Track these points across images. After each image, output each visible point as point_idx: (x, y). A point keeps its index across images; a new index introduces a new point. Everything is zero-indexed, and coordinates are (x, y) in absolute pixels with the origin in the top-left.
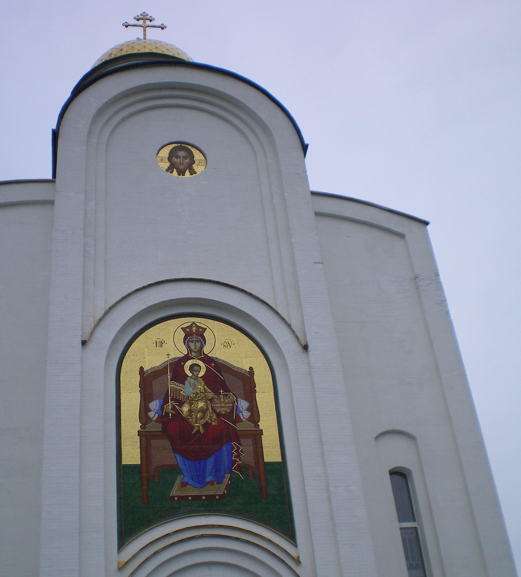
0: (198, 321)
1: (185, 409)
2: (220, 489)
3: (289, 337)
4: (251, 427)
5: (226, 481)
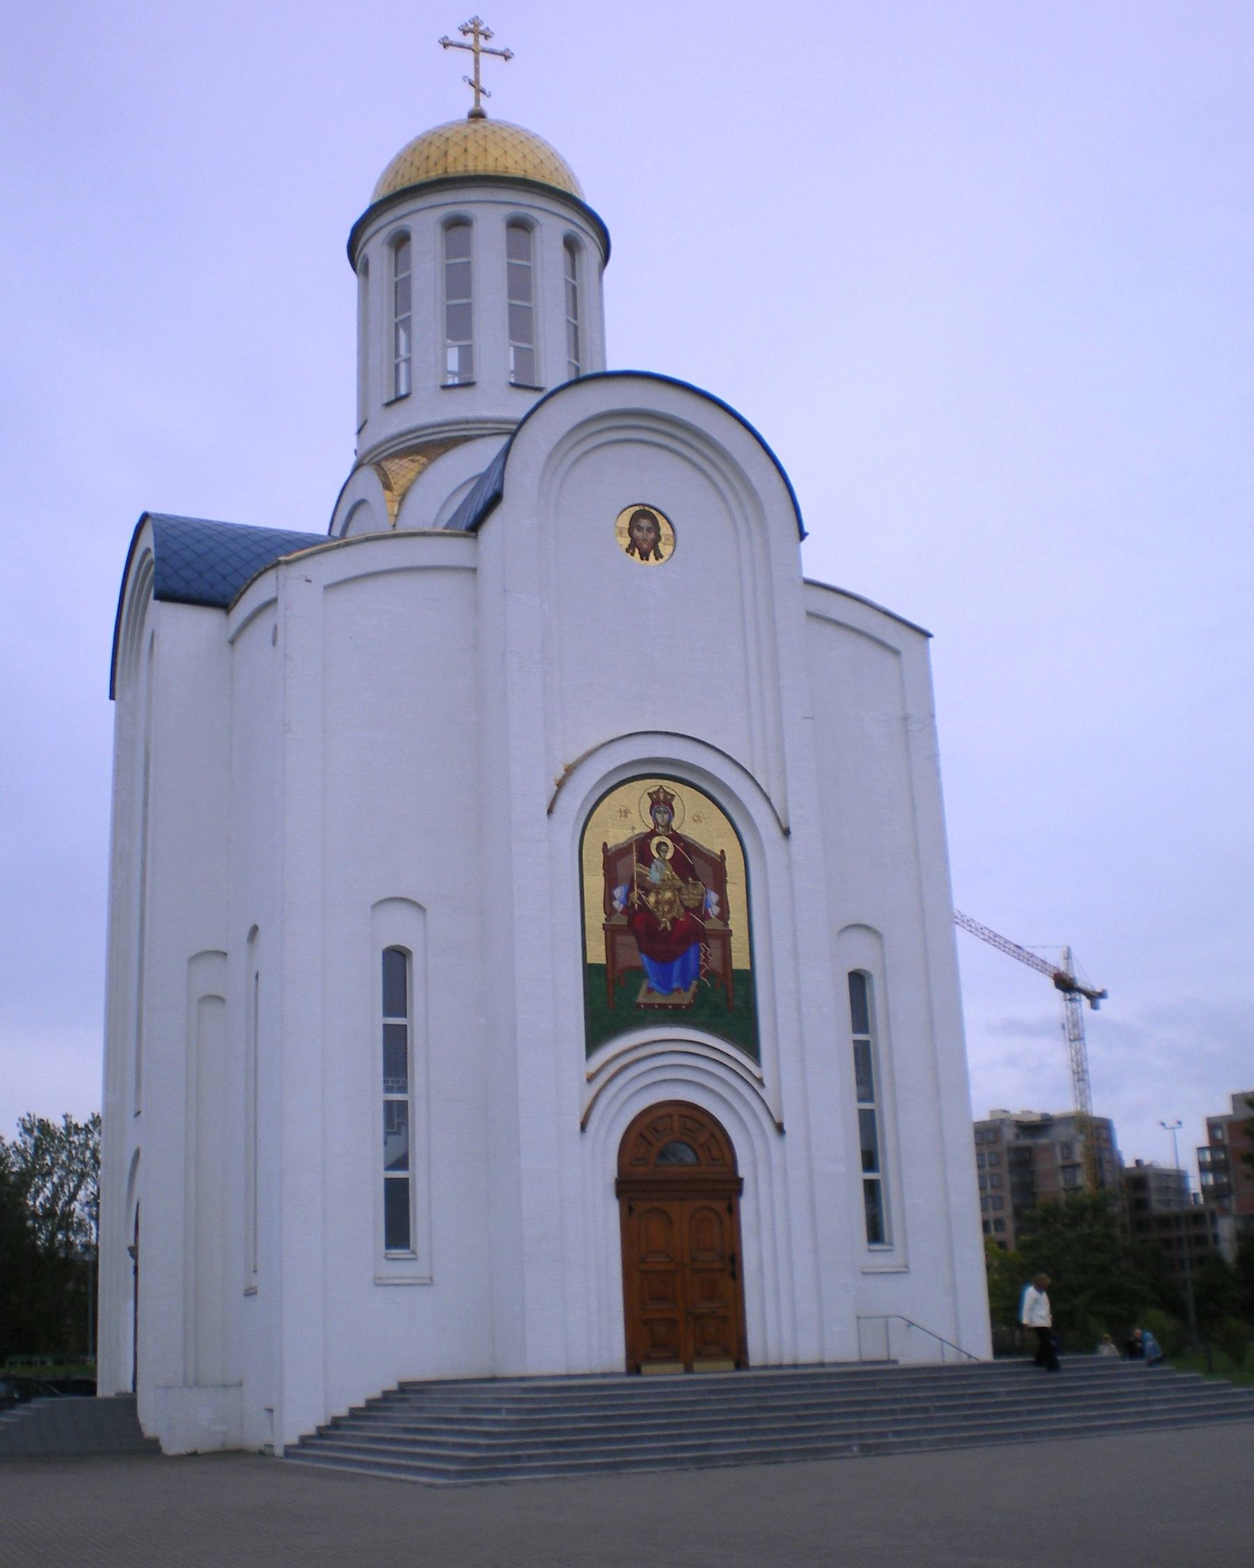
0: (666, 784)
1: (652, 899)
2: (685, 998)
3: (769, 818)
4: (718, 925)
5: (693, 988)
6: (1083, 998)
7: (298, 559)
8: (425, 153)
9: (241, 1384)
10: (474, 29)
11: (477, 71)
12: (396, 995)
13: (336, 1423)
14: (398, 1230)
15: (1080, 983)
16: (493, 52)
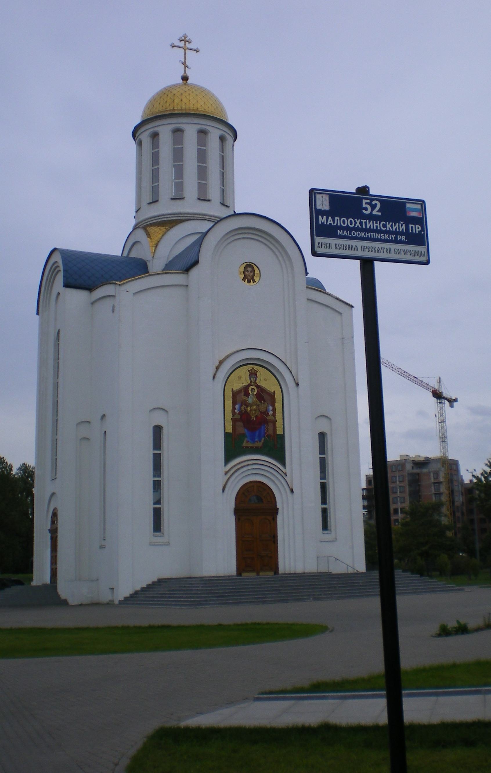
1: (249, 409)
2: (260, 444)
6: (446, 401)
7: (124, 284)
8: (165, 100)
9: (98, 580)
10: (185, 39)
11: (185, 58)
12: (157, 443)
13: (136, 593)
14: (157, 526)
15: (445, 395)
16: (192, 49)
